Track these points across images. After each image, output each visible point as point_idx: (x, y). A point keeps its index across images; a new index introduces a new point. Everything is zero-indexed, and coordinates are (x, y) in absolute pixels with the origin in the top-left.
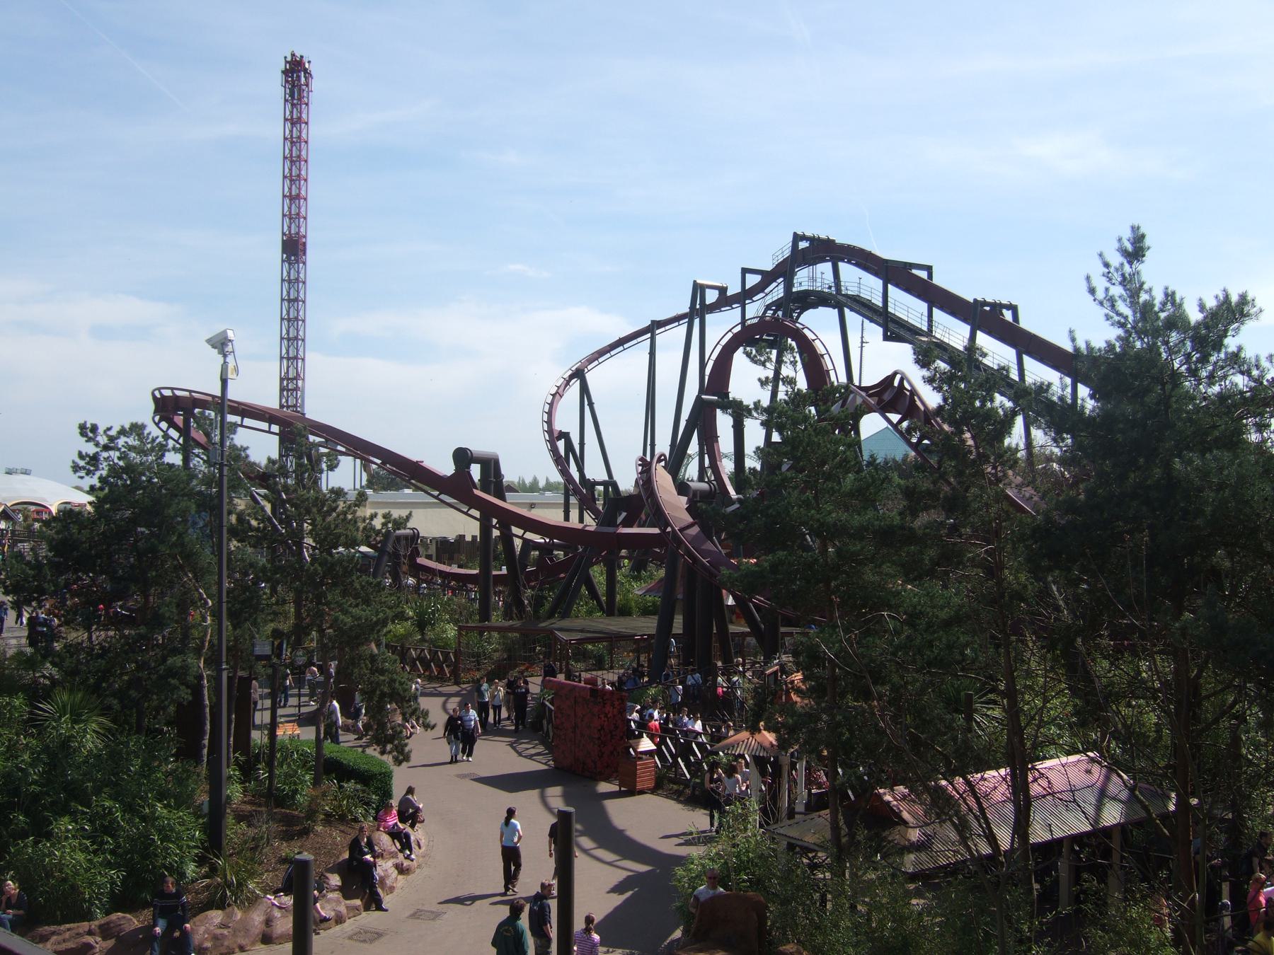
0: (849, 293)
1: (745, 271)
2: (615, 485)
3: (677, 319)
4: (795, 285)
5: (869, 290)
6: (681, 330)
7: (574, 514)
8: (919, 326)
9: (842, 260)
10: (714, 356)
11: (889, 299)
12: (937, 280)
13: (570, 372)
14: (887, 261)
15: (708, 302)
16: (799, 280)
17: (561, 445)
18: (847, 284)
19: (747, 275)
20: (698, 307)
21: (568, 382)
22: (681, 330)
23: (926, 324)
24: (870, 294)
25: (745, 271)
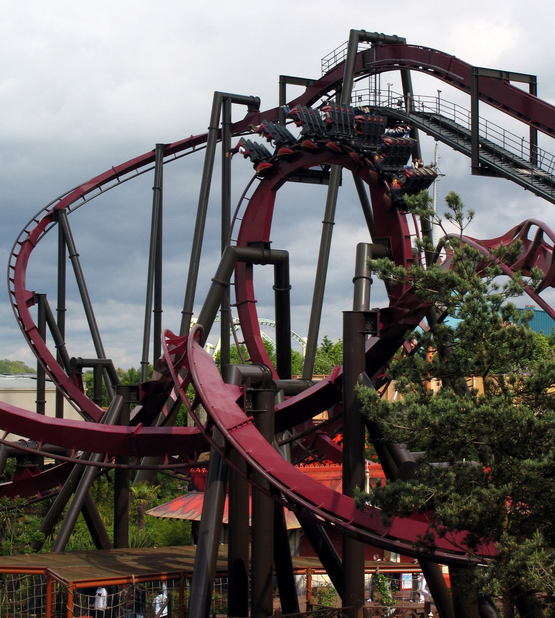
0: (426, 110)
1: (284, 80)
2: (109, 366)
3: (192, 142)
4: (354, 100)
5: (501, 132)
6: (201, 154)
7: (51, 399)
8: (519, 154)
9: (416, 68)
10: (241, 215)
11: (480, 120)
12: (542, 95)
13: (45, 214)
14: (477, 69)
15: (234, 120)
16: (359, 93)
17: (34, 310)
18: (422, 99)
19: (288, 86)
20: (220, 126)
21: (42, 227)
22: (201, 154)
23: (528, 152)
24: (452, 112)
25: (284, 80)
